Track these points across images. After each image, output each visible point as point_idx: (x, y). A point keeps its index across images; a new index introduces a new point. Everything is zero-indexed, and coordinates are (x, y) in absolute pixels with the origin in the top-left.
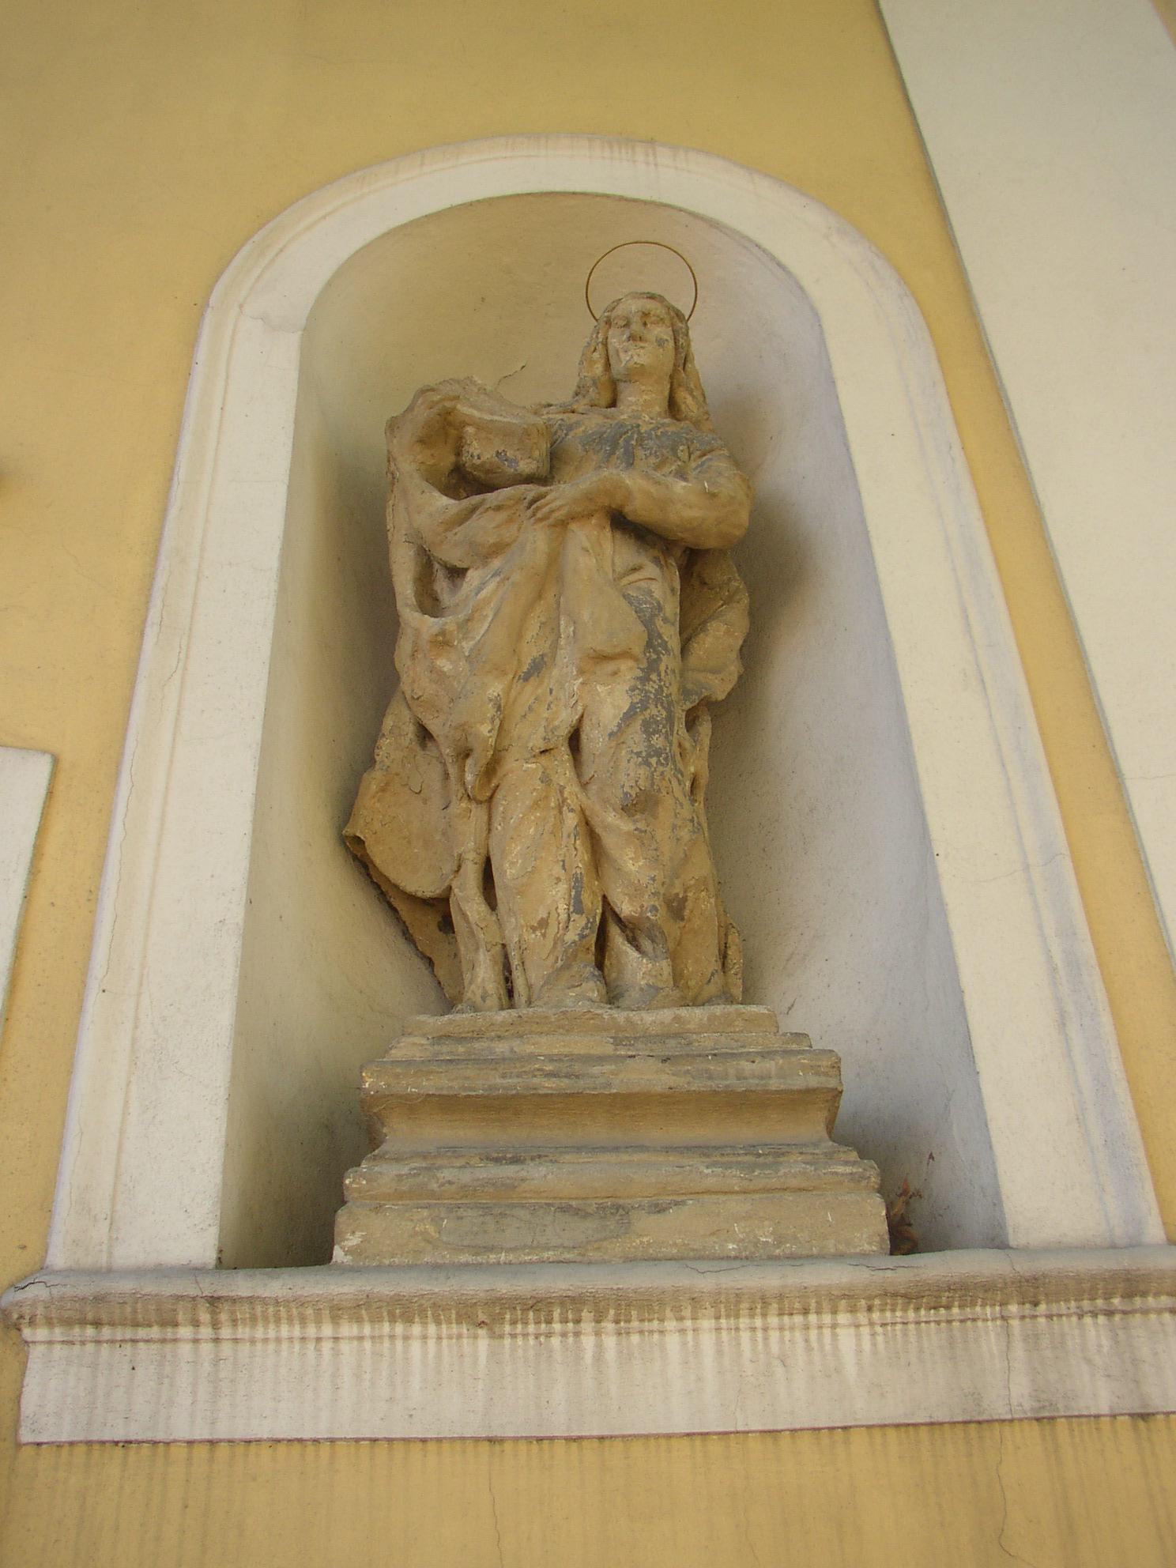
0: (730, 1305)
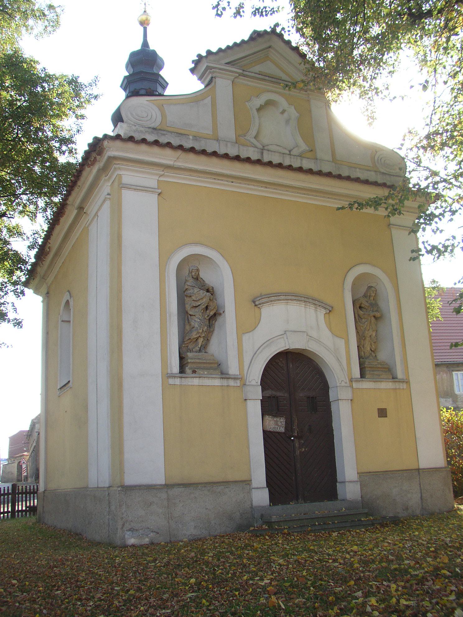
0: (386, 381)
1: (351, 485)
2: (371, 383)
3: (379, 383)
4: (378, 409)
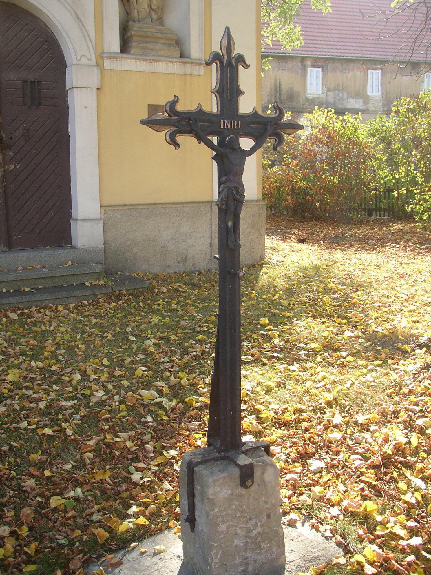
0: (166, 61)
1: (87, 225)
2: (139, 63)
3: (154, 64)
4: (149, 106)
